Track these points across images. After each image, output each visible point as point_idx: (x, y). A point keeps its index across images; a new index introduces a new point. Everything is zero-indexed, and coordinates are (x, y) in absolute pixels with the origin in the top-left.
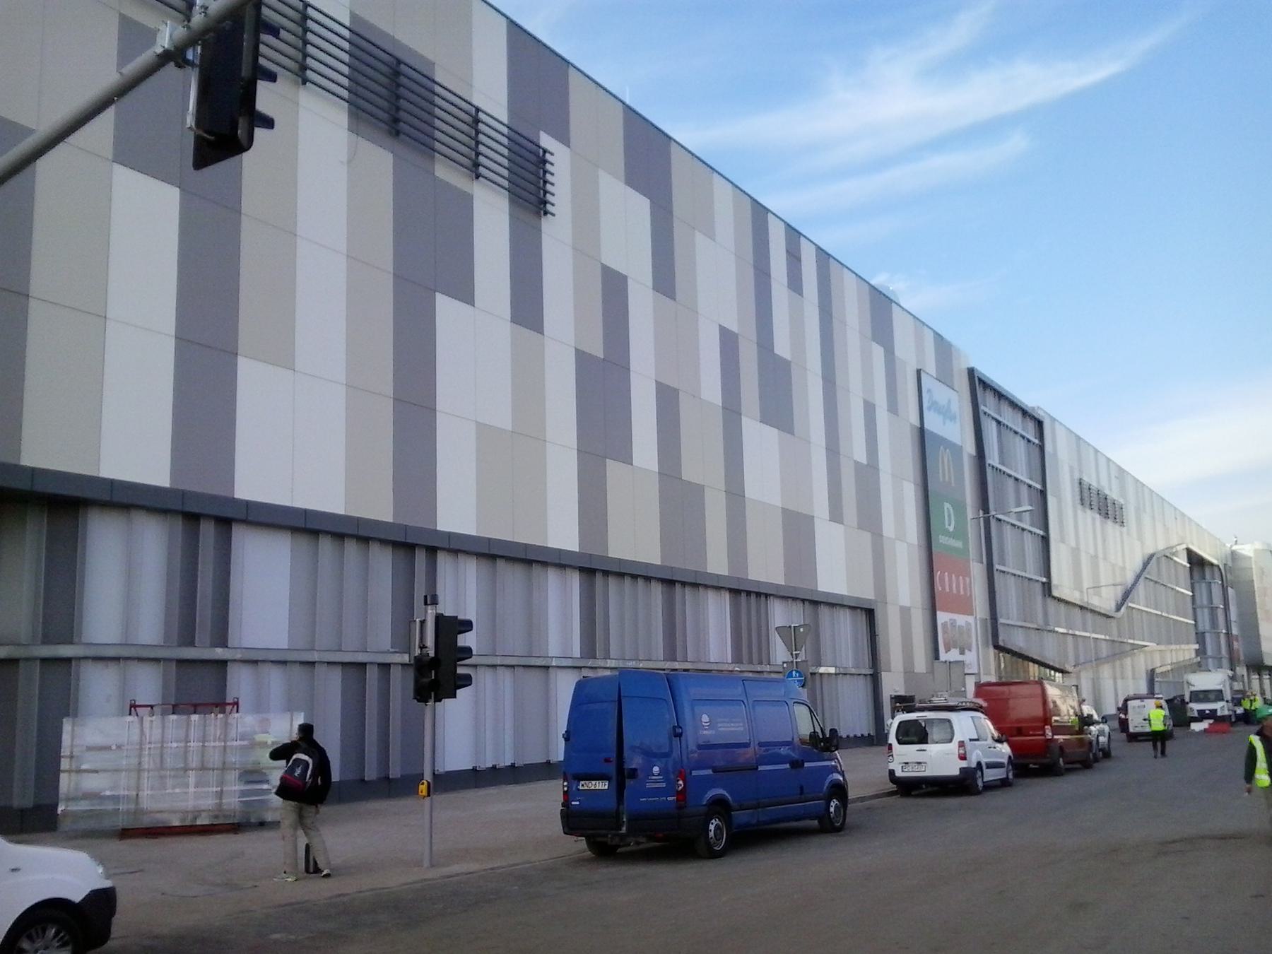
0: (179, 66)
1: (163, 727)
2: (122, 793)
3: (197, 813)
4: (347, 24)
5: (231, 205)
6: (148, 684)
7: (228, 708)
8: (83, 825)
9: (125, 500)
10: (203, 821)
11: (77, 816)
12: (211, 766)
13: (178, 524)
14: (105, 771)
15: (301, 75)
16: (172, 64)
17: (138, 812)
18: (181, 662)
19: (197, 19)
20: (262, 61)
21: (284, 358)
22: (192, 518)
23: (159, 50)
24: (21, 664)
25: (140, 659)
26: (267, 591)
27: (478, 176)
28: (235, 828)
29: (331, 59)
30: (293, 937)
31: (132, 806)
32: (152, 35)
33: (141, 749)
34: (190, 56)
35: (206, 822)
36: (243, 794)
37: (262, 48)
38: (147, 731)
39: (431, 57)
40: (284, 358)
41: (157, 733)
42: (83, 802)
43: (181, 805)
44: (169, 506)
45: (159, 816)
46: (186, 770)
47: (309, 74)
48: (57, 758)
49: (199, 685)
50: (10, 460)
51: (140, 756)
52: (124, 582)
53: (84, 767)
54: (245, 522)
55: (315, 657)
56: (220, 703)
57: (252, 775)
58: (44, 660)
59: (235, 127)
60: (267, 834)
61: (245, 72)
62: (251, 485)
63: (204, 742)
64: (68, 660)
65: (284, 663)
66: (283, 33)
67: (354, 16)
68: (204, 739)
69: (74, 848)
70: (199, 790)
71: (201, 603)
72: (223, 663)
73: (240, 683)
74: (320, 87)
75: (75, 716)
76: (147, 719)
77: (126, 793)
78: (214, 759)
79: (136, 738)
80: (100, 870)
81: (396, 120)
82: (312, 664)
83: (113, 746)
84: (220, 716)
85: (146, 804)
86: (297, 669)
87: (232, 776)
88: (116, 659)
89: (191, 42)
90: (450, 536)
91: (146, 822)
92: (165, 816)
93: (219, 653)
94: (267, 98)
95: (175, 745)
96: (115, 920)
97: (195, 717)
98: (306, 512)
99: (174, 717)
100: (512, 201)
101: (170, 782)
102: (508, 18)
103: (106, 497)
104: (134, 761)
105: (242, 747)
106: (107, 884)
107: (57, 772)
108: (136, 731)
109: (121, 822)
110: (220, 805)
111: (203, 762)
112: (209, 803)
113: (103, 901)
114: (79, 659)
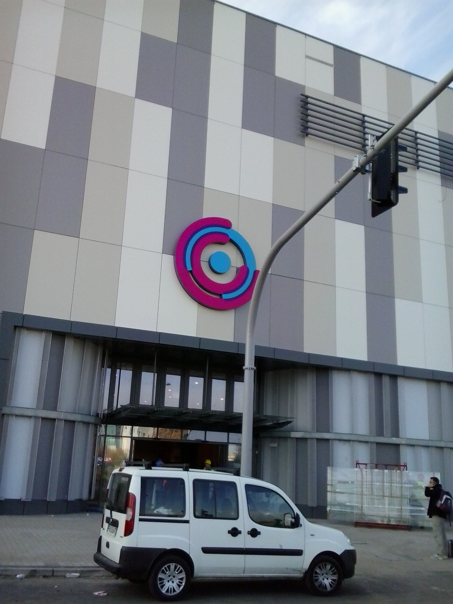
0: (363, 174)
1: (372, 475)
2: (355, 505)
3: (389, 518)
4: (437, 137)
5: (388, 230)
6: (363, 453)
7: (402, 468)
8: (338, 518)
9: (348, 367)
10: (393, 523)
11: (335, 513)
12: (395, 495)
13: (372, 378)
14: (346, 493)
15: (417, 165)
16: (360, 173)
17: (362, 514)
18: (378, 444)
19: (370, 152)
20: (400, 164)
21: (418, 298)
22: (379, 375)
23: (354, 169)
24: (309, 440)
25: (340, 440)
26: (416, 409)
27: (418, 167)
28: (409, 528)
29: (430, 154)
30: (443, 590)
31: (360, 512)
32: (351, 162)
33: (362, 484)
34: (367, 168)
35: (394, 523)
36: (411, 511)
37: (400, 158)
38: (365, 476)
39: (302, 83)
40: (418, 298)
41: (369, 478)
42: (338, 507)
43: (382, 513)
44: (367, 370)
45: (372, 517)
46: (384, 496)
47: (420, 164)
48: (326, 485)
49: (387, 455)
50: (395, 364)
51: (362, 488)
52: (350, 405)
53: (337, 490)
54: (404, 377)
55: (442, 444)
56: (397, 465)
57: (414, 501)
58: (318, 440)
59: (389, 195)
60: (425, 533)
61: (392, 170)
62: (405, 358)
63: (391, 483)
64: (327, 440)
65: (428, 447)
66: (409, 149)
67: (440, 132)
68: (391, 482)
69: (336, 528)
70: (390, 507)
71: (386, 416)
72: (397, 446)
73: (407, 455)
74: (326, 139)
75: (332, 466)
76: (364, 470)
77: (357, 505)
78: (398, 493)
79: (359, 478)
80: (349, 541)
81: (417, 161)
82: (442, 448)
83: (349, 481)
84: (398, 471)
85: (366, 511)
86: (434, 451)
87: (406, 501)
88: (349, 441)
89: (367, 162)
90: (404, 368)
91: (366, 520)
92: (375, 518)
93: (395, 440)
94: (403, 180)
95: (378, 484)
96: (357, 567)
97: (386, 471)
98: (433, 372)
99: (376, 470)
100: (442, 178)
101: (376, 502)
102: (334, 45)
103: (340, 366)
104: (360, 490)
105: (410, 488)
106: (352, 548)
107: (326, 491)
108: (359, 475)
109: (355, 519)
110: (401, 515)
111: (391, 494)
112: (394, 514)
113: (350, 555)
114: (333, 440)
